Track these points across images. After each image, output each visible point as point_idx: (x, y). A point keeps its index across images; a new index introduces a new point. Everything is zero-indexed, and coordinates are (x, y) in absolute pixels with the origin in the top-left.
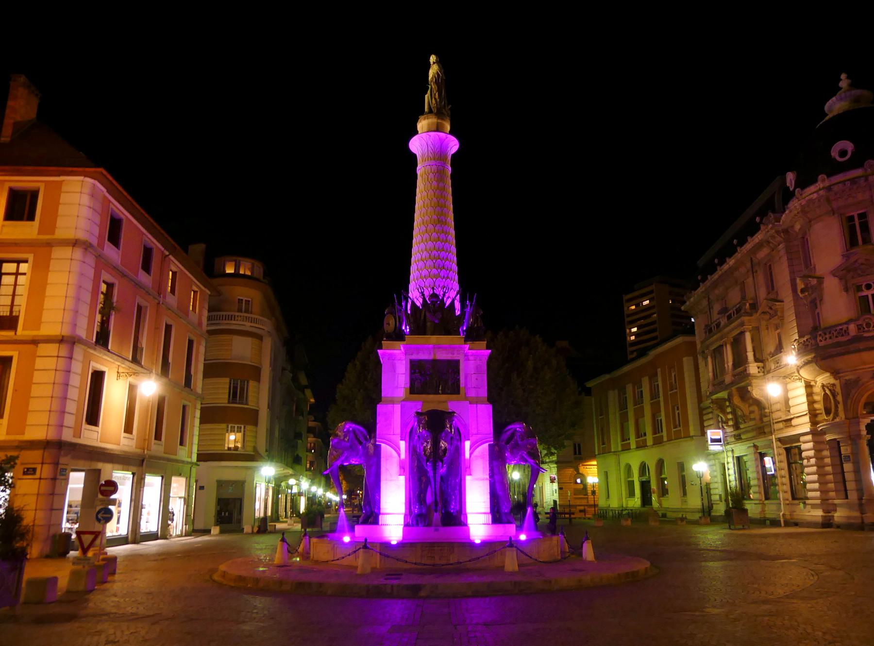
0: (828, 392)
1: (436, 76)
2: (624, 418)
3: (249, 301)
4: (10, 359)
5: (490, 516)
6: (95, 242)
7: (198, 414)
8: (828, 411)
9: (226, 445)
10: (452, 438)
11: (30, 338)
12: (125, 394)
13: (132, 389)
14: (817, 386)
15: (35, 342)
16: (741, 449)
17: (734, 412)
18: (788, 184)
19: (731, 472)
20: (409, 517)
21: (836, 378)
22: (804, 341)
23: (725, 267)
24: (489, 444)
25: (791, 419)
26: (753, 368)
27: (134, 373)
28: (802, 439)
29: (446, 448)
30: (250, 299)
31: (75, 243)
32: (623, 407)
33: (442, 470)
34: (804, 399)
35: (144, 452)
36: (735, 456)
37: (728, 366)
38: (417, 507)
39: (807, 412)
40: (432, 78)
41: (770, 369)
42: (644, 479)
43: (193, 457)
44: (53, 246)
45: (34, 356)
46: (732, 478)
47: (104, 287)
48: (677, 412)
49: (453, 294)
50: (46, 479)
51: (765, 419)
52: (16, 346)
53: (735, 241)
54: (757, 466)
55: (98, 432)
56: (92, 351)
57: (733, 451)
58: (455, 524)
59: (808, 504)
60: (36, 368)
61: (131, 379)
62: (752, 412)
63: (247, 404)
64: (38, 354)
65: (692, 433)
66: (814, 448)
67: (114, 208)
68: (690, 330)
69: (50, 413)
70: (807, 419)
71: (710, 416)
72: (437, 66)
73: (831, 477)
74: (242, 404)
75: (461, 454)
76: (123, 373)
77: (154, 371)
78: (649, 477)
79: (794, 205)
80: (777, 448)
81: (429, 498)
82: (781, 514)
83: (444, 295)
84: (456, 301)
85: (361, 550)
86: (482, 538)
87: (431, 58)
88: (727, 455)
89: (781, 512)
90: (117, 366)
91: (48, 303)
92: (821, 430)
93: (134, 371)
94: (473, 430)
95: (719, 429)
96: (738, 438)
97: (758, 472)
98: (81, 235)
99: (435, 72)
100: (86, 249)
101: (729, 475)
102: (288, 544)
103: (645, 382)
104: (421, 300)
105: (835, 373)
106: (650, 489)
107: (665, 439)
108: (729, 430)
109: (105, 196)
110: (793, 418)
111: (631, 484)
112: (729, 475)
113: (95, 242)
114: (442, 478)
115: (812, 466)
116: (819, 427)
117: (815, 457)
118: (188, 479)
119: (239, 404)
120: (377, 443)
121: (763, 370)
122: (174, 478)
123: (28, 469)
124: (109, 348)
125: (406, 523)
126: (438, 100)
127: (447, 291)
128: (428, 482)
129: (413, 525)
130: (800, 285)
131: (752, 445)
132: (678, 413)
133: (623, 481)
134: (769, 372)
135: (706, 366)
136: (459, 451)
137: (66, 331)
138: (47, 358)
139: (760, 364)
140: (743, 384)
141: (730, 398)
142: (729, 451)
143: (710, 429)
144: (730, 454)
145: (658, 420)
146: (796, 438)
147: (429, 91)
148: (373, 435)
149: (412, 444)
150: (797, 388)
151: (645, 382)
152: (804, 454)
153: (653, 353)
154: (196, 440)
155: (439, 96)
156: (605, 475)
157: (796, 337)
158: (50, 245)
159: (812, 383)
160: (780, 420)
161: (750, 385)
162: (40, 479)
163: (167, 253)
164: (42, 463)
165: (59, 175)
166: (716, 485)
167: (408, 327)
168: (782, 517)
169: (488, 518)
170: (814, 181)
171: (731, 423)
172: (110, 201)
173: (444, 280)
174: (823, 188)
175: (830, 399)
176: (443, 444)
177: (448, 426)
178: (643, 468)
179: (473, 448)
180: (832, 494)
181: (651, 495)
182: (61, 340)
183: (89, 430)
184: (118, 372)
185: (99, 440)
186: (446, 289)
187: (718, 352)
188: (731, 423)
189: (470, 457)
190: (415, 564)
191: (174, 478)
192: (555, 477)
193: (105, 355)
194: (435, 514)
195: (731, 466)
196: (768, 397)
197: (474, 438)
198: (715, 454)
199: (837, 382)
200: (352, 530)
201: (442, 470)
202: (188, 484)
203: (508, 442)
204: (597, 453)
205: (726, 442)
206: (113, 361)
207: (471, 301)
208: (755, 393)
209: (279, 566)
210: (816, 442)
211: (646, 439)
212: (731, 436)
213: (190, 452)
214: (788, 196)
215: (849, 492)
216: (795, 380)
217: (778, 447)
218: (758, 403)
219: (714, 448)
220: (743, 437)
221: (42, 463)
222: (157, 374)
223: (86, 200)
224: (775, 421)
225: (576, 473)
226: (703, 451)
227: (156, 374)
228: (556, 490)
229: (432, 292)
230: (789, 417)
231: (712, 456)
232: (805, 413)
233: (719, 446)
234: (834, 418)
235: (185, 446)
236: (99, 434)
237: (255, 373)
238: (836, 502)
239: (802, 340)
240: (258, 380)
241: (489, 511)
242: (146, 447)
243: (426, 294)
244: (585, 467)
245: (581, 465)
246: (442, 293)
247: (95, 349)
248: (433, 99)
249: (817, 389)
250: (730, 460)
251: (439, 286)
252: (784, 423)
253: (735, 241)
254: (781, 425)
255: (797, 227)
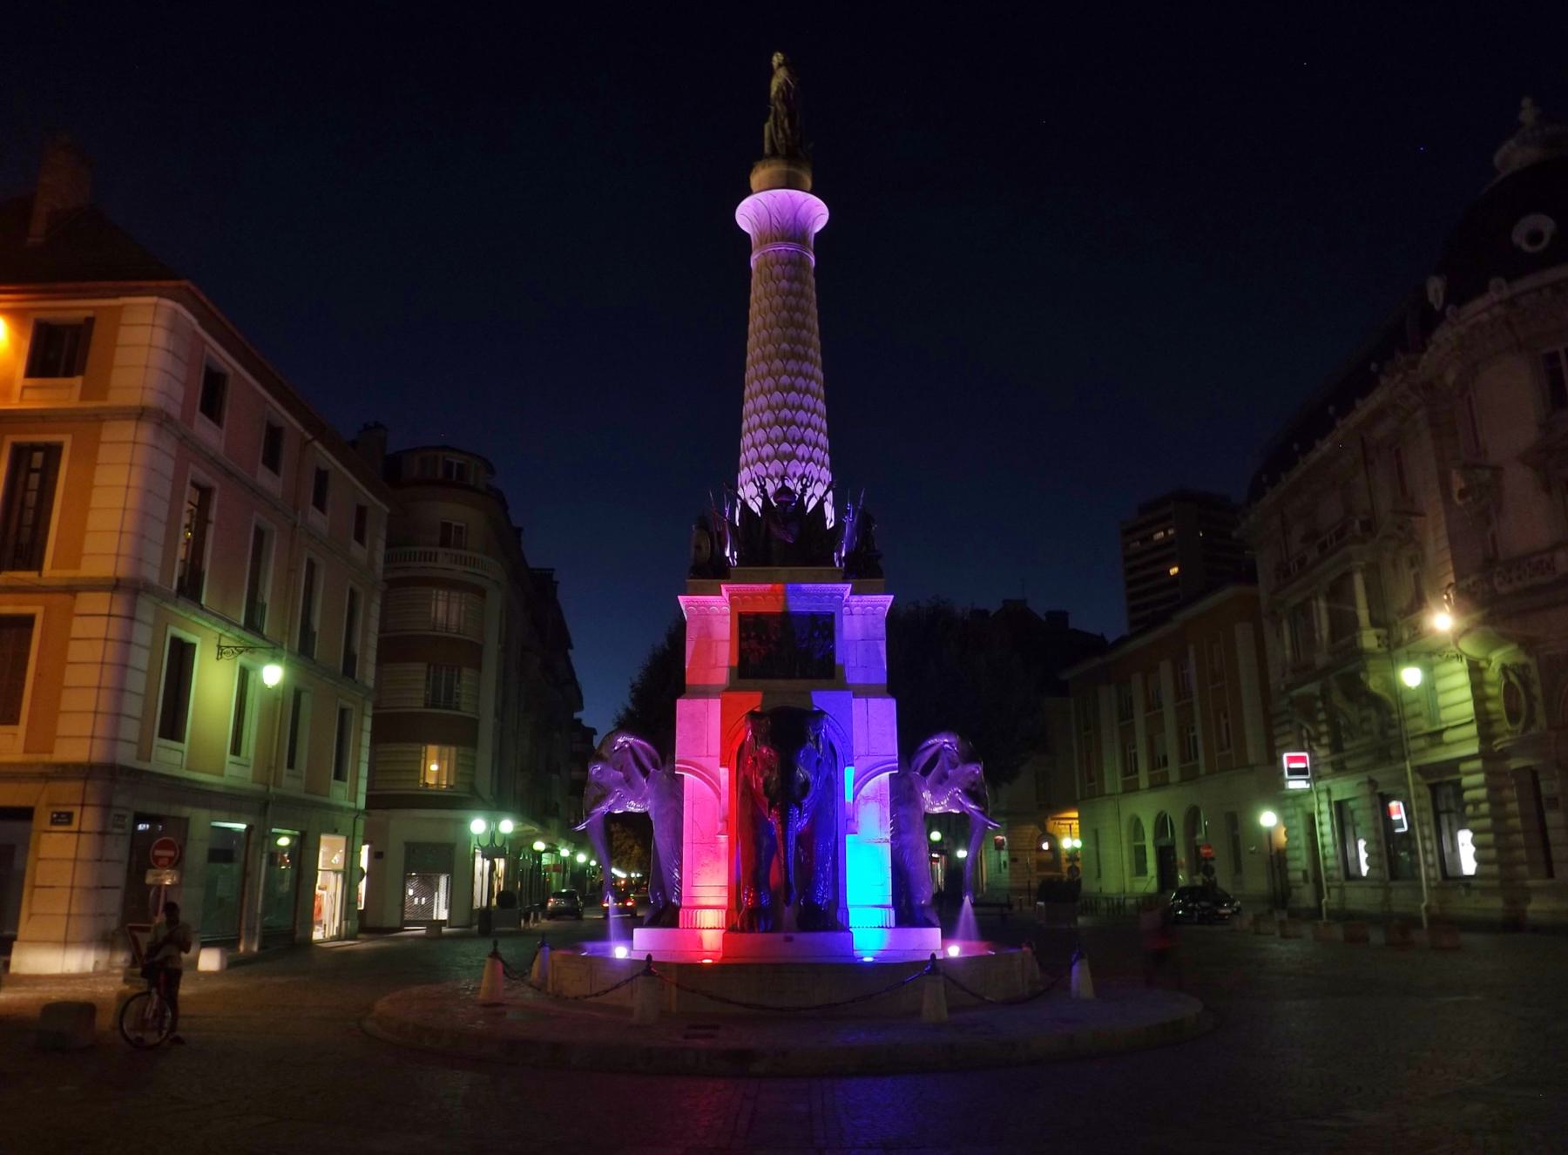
0: (1513, 678)
1: (784, 88)
2: (1127, 734)
3: (461, 528)
4: (28, 621)
5: (892, 912)
6: (176, 411)
7: (368, 724)
8: (1513, 716)
9: (422, 781)
10: (819, 760)
11: (65, 583)
12: (233, 684)
13: (244, 675)
14: (1491, 669)
15: (72, 589)
16: (1343, 788)
17: (1332, 721)
18: (1431, 299)
19: (1327, 828)
20: (735, 913)
21: (1528, 653)
22: (1468, 586)
23: (1314, 456)
24: (890, 775)
25: (1441, 732)
26: (1369, 639)
27: (247, 649)
28: (1464, 767)
29: (807, 780)
30: (463, 525)
31: (140, 414)
32: (1126, 714)
33: (800, 824)
34: (1467, 693)
35: (268, 790)
36: (1333, 800)
37: (1321, 637)
38: (1171, 532)
39: (1473, 717)
40: (777, 92)
41: (1401, 639)
42: (1163, 842)
43: (358, 802)
44: (104, 420)
45: (70, 614)
46: (1328, 840)
47: (191, 494)
48: (1223, 722)
49: (819, 490)
50: (90, 833)
51: (1392, 732)
52: (39, 597)
53: (1331, 409)
54: (1376, 818)
55: (182, 752)
56: (170, 607)
57: (1329, 791)
58: (826, 929)
59: (1475, 888)
60: (73, 635)
61: (241, 659)
62: (1364, 720)
63: (457, 709)
64: (77, 611)
65: (1252, 760)
66: (1486, 784)
67: (212, 353)
68: (1248, 575)
69: (95, 717)
70: (1472, 730)
71: (1287, 728)
72: (786, 72)
73: (1519, 838)
74: (450, 708)
75: (1391, 812)
76: (228, 647)
77: (285, 647)
78: (1173, 840)
79: (1444, 335)
80: (1414, 784)
81: (775, 877)
82: (1423, 905)
83: (804, 490)
84: (826, 504)
85: (641, 978)
86: (875, 953)
87: (775, 58)
88: (1318, 799)
89: (1422, 902)
90: (217, 636)
91: (94, 521)
92: (1501, 750)
93: (248, 645)
94: (859, 747)
95: (1303, 750)
96: (1339, 768)
97: (1377, 830)
98: (150, 399)
99: (781, 80)
100: (160, 425)
101: (1322, 835)
102: (503, 962)
103: (1166, 669)
104: (760, 501)
105: (1527, 645)
106: (1175, 860)
107: (1202, 770)
108: (1322, 753)
109: (195, 332)
110: (1447, 729)
111: (1140, 853)
112: (1322, 835)
113: (176, 411)
114: (798, 838)
115: (1483, 816)
116: (1496, 746)
117: (1489, 799)
118: (351, 839)
119: (445, 708)
120: (676, 772)
121: (1386, 642)
122: (324, 838)
123: (59, 814)
124: (203, 602)
125: (730, 925)
126: (788, 132)
127: (808, 484)
128: (773, 848)
129: (742, 930)
130: (1458, 483)
131: (1366, 779)
132: (1227, 725)
133: (1125, 845)
134: (1399, 644)
135: (1278, 635)
136: (833, 786)
137: (123, 570)
138: (91, 618)
139: (1382, 632)
140: (1351, 668)
141: (1325, 695)
142: (1322, 791)
143: (1289, 751)
144: (1324, 797)
145: (1189, 738)
146: (1453, 765)
147: (771, 118)
148: (668, 757)
149: (742, 774)
150: (1453, 673)
151: (1166, 669)
152: (1468, 795)
153: (1181, 617)
154: (364, 771)
155: (790, 124)
156: (1090, 832)
157: (1451, 579)
158: (99, 418)
159: (1483, 664)
160: (1420, 733)
161: (1364, 669)
162: (79, 832)
163: (310, 437)
164: (83, 805)
165: (117, 297)
166: (1297, 854)
167: (735, 553)
168: (1423, 913)
169: (888, 916)
170: (1483, 290)
171: (1325, 740)
172: (204, 342)
173: (804, 464)
174: (1500, 302)
175: (1517, 690)
176: (802, 774)
177: (812, 738)
178: (1162, 824)
179: (860, 781)
180: (1523, 869)
181: (1176, 872)
182: (115, 586)
183: (166, 747)
184: (219, 647)
185: (184, 766)
186: (808, 480)
187: (1303, 611)
188: (1325, 740)
189: (854, 799)
190: (746, 1005)
191: (324, 838)
192: (1003, 840)
193: (195, 614)
194: (786, 908)
195: (1326, 818)
196: (1396, 689)
197: (865, 763)
198: (1297, 796)
199: (1532, 662)
200: (629, 937)
201: (800, 824)
202: (350, 849)
203: (926, 771)
204: (1078, 797)
205: (1316, 775)
206: (210, 626)
207: (855, 503)
208: (1374, 684)
209: (485, 1006)
210: (1490, 773)
211: (1167, 772)
212: (1326, 764)
213: (353, 793)
214: (1430, 320)
215: (1556, 866)
216: (1449, 659)
217: (1416, 784)
218: (1376, 702)
219: (1297, 785)
220: (1349, 765)
221: (83, 805)
222: (290, 652)
223: (160, 337)
224: (1410, 736)
225: (1041, 833)
226: (1273, 792)
227: (288, 651)
228: (1005, 863)
229: (780, 486)
230: (1438, 727)
231: (1289, 802)
232: (1469, 719)
233: (1304, 782)
234: (1525, 729)
235: (345, 780)
236: (185, 754)
237: (472, 653)
238: (1531, 883)
239: (1463, 584)
240: (478, 667)
241: (889, 901)
242: (272, 781)
243: (770, 488)
244: (1057, 822)
245: (1049, 818)
246: (799, 487)
247: (176, 605)
248: (780, 131)
249: (1493, 674)
250: (1324, 807)
251: (795, 475)
252: (1428, 739)
253: (1331, 409)
254: (1422, 743)
255: (1451, 377)
